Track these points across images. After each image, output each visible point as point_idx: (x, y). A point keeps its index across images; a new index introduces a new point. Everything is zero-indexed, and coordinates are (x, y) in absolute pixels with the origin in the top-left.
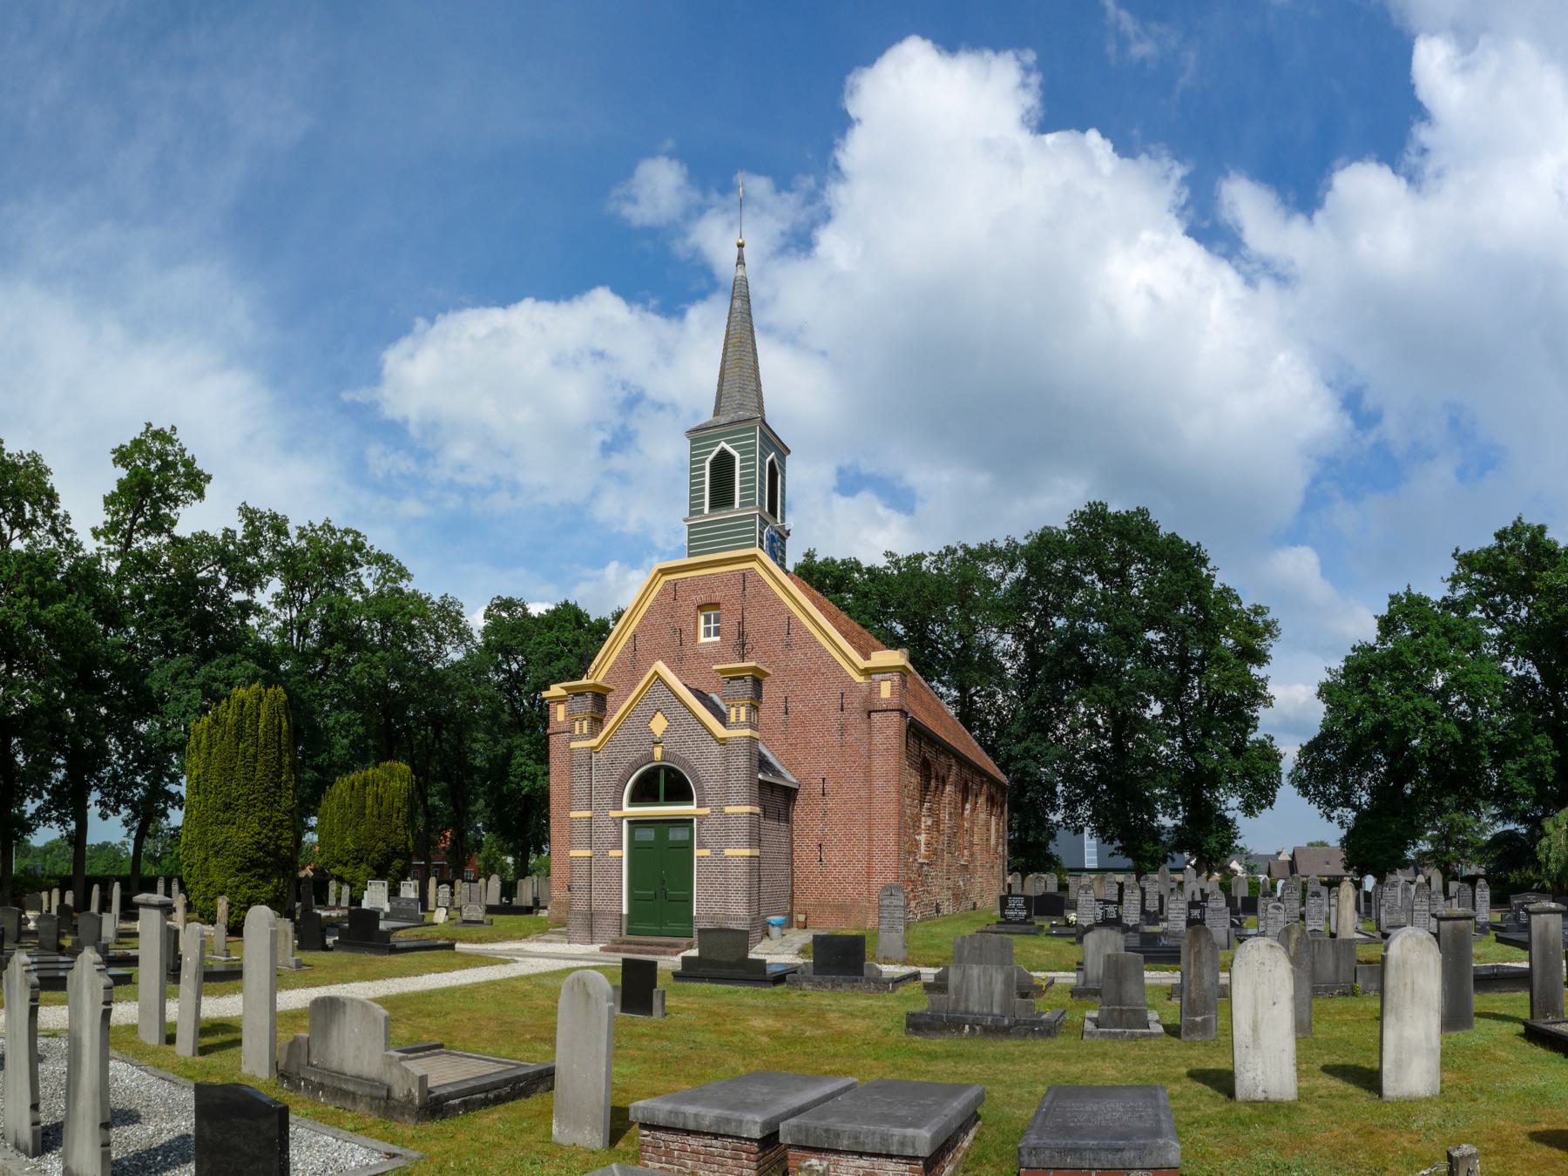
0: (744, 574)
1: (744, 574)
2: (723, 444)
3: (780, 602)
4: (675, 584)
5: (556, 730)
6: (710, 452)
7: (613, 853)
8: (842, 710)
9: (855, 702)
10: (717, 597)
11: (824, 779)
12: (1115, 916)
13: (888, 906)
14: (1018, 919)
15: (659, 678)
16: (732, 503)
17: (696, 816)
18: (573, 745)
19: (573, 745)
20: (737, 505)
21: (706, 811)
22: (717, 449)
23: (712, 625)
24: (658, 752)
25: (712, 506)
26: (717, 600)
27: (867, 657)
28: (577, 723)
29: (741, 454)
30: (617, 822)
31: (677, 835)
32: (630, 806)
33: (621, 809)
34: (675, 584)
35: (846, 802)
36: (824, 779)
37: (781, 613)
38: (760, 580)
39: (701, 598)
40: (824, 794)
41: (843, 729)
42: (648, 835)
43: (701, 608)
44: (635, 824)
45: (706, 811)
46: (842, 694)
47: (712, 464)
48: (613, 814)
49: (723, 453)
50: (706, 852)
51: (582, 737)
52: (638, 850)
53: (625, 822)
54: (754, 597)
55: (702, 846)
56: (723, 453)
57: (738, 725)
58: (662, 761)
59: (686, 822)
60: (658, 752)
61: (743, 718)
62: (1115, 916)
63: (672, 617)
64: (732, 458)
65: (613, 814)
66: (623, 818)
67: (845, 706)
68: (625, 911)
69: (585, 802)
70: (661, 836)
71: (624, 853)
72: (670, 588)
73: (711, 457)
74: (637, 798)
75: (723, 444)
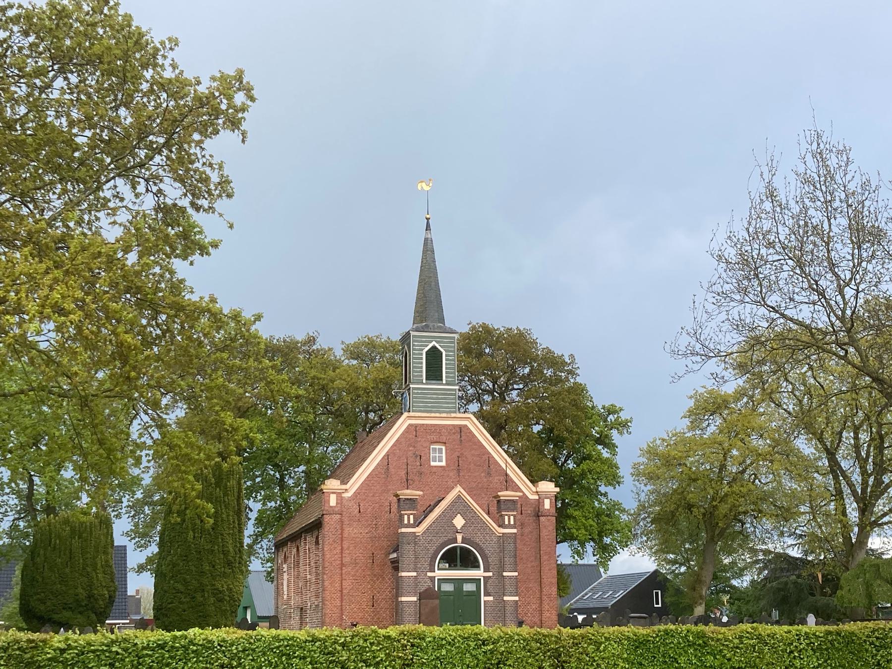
0: (460, 428)
2: (434, 343)
19: (404, 530)
20: (444, 382)
21: (490, 574)
24: (459, 537)
31: (469, 587)
37: (484, 455)
38: (471, 432)
39: (434, 437)
45: (490, 574)
47: (427, 353)
48: (429, 574)
49: (434, 347)
50: (491, 598)
51: (409, 526)
55: (487, 594)
56: (434, 347)
57: (509, 526)
61: (512, 522)
65: (429, 574)
69: (412, 566)
73: (427, 349)
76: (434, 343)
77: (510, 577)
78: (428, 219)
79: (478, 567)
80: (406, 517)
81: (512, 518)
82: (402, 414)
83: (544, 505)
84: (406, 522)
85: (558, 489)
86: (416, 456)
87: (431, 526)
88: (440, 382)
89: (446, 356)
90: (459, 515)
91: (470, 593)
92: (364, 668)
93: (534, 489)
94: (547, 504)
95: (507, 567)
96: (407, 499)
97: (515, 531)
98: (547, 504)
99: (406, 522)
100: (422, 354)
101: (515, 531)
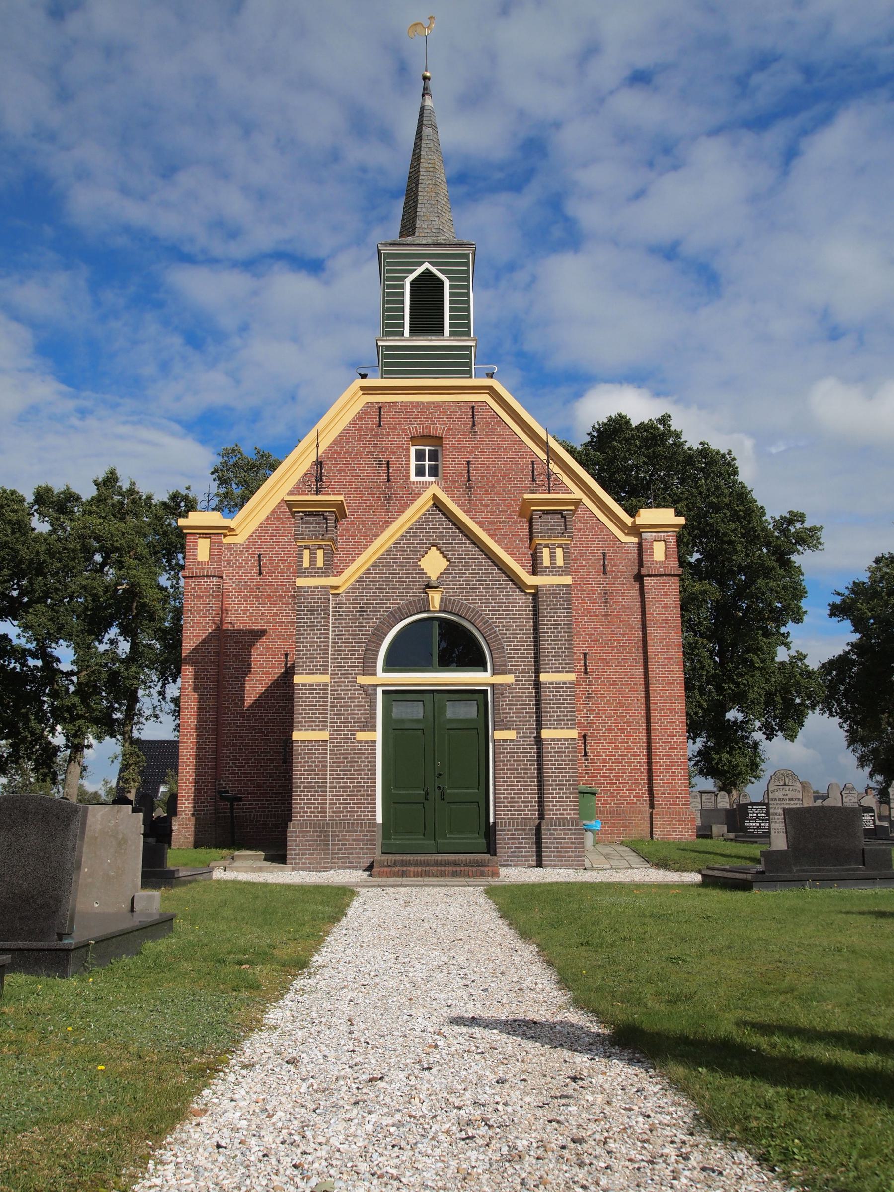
0: (473, 408)
1: (473, 408)
2: (426, 265)
3: (522, 444)
4: (380, 408)
5: (197, 572)
6: (412, 271)
7: (361, 736)
8: (605, 572)
9: (625, 565)
10: (438, 429)
11: (585, 655)
12: (872, 827)
13: (780, 799)
14: (760, 832)
15: (437, 504)
16: (441, 331)
17: (493, 685)
18: (301, 582)
19: (301, 582)
21: (509, 679)
22: (420, 270)
23: (427, 463)
24: (435, 599)
25: (413, 331)
26: (439, 433)
27: (632, 511)
28: (306, 553)
29: (450, 279)
30: (368, 692)
32: (385, 671)
33: (375, 675)
34: (380, 408)
35: (615, 684)
36: (585, 655)
39: (417, 428)
40: (586, 673)
41: (607, 597)
42: (415, 711)
43: (416, 439)
44: (393, 696)
45: (509, 679)
46: (604, 554)
47: (413, 283)
48: (362, 680)
49: (427, 273)
50: (510, 734)
51: (313, 571)
52: (397, 732)
53: (380, 691)
54: (487, 435)
56: (427, 273)
57: (554, 570)
58: (440, 611)
59: (478, 695)
60: (435, 599)
61: (560, 562)
62: (872, 827)
63: (376, 446)
64: (441, 283)
65: (362, 680)
66: (377, 686)
67: (608, 568)
68: (379, 820)
70: (437, 711)
71: (378, 735)
72: (374, 413)
74: (392, 664)
75: (433, 270)
76: (426, 265)
77: (558, 686)
78: (425, 79)
79: (486, 671)
80: (306, 553)
81: (559, 552)
82: (362, 686)
83: (652, 554)
84: (306, 564)
85: (682, 520)
86: (380, 464)
87: (367, 572)
88: (441, 338)
89: (451, 287)
90: (434, 549)
91: (464, 726)
92: (422, 1190)
93: (628, 520)
94: (659, 552)
95: (365, 816)
96: (310, 514)
97: (567, 580)
98: (659, 552)
99: (306, 564)
100: (402, 286)
101: (567, 580)
